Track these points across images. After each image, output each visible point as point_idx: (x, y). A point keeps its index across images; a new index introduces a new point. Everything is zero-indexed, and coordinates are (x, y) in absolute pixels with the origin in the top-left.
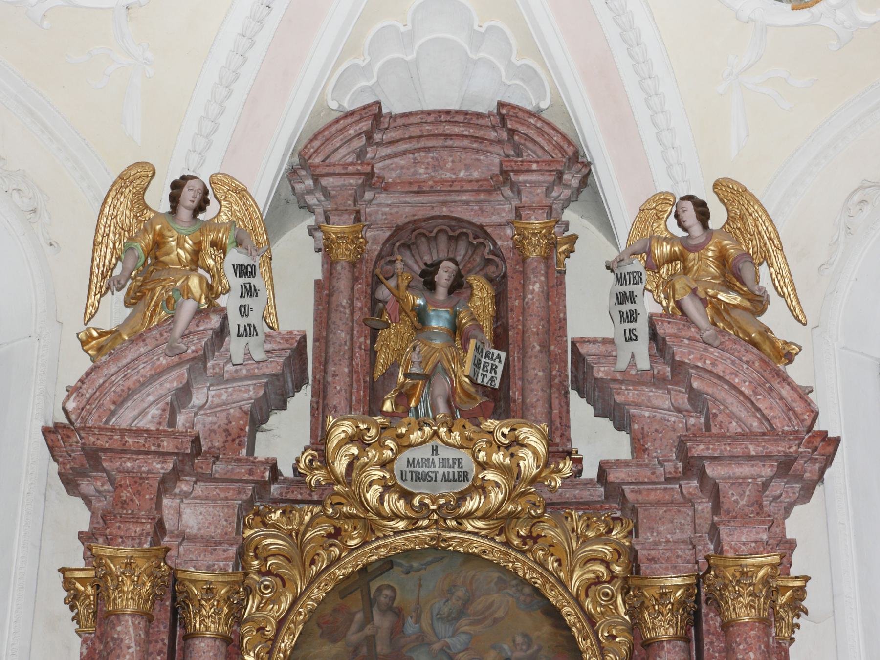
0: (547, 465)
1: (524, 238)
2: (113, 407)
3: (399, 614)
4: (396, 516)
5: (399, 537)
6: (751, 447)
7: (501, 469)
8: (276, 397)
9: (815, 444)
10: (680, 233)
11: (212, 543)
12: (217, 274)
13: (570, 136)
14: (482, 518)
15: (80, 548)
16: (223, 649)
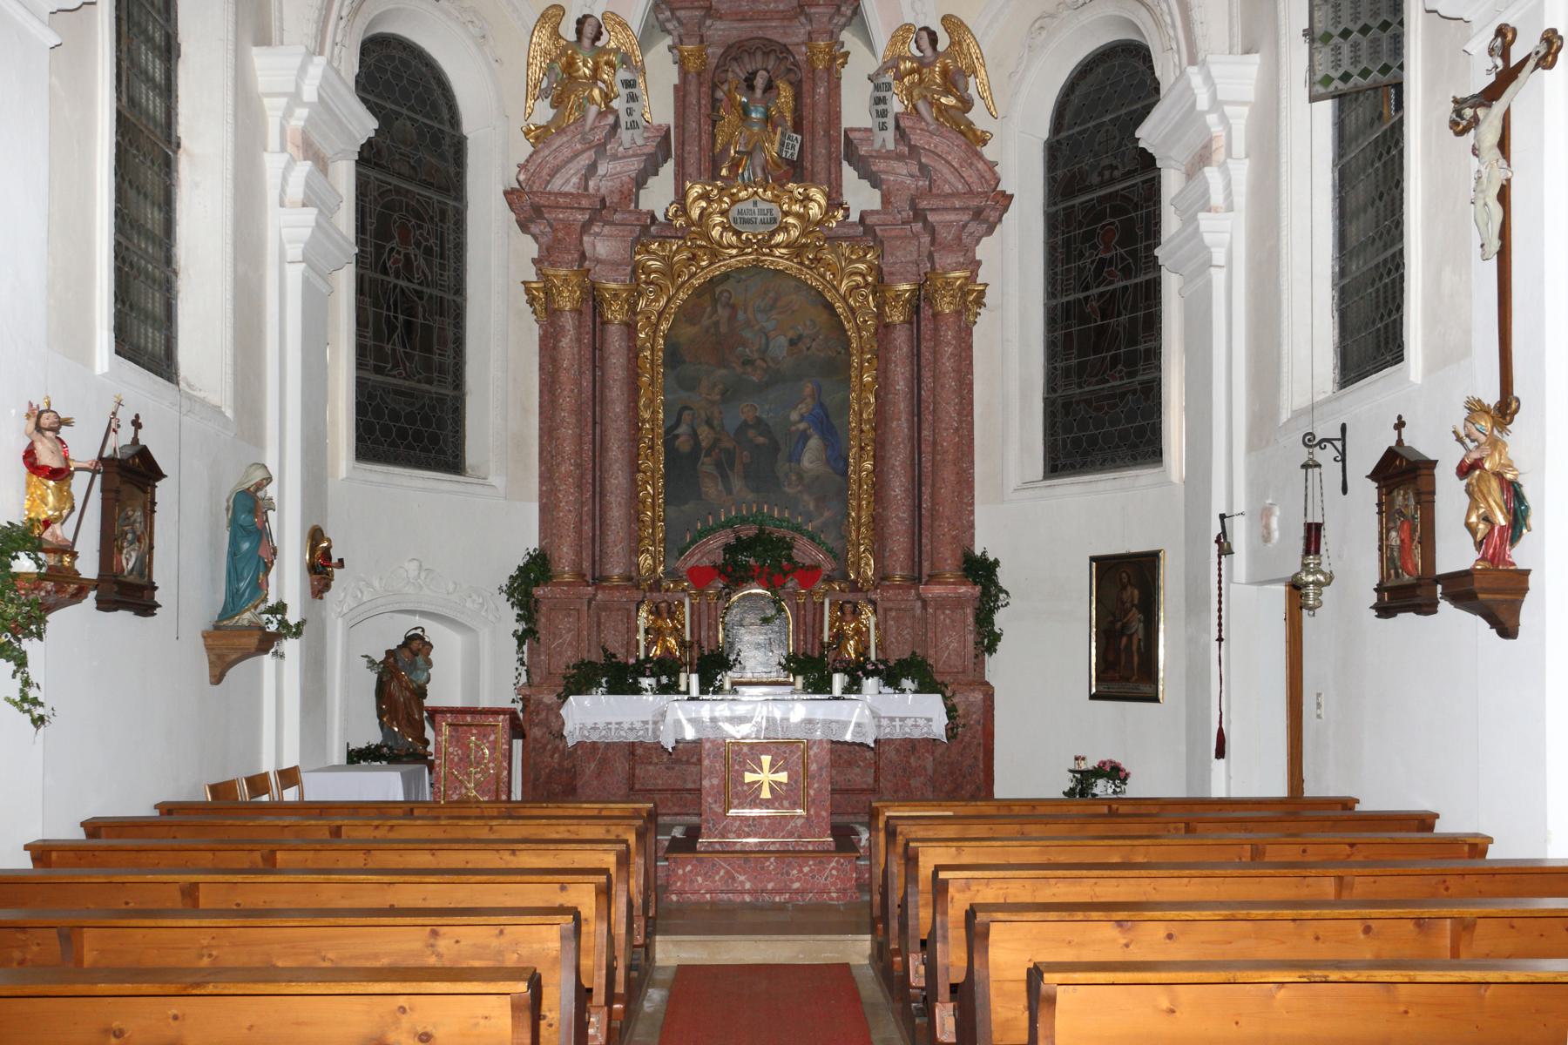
3: (734, 308)
4: (731, 246)
5: (732, 259)
7: (798, 215)
8: (651, 167)
10: (918, 54)
11: (615, 265)
12: (610, 85)
15: (534, 269)
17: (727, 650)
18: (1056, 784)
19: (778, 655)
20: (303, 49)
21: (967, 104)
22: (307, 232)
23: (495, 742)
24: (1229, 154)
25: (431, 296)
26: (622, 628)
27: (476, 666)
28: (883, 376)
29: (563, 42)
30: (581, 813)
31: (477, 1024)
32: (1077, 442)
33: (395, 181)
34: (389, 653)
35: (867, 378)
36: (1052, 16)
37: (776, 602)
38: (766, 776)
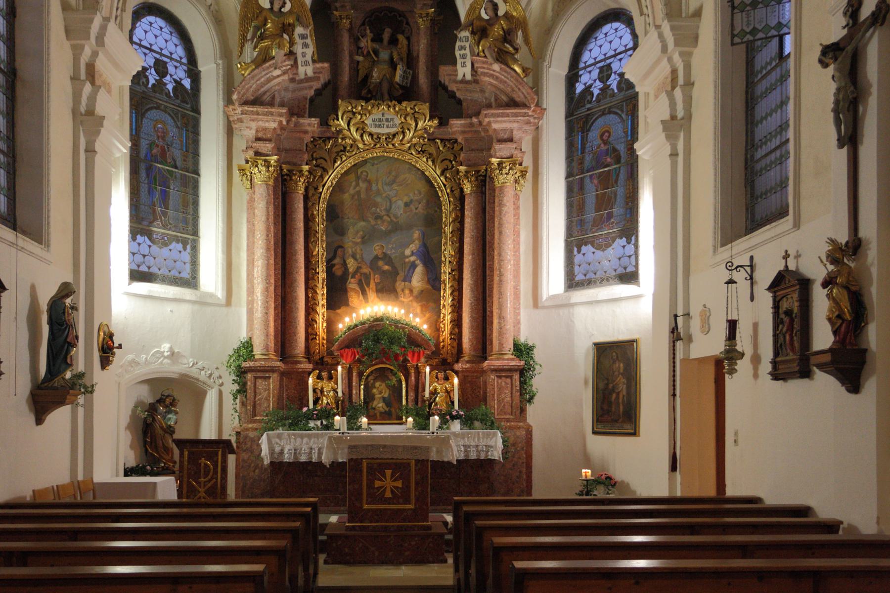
3: (369, 182)
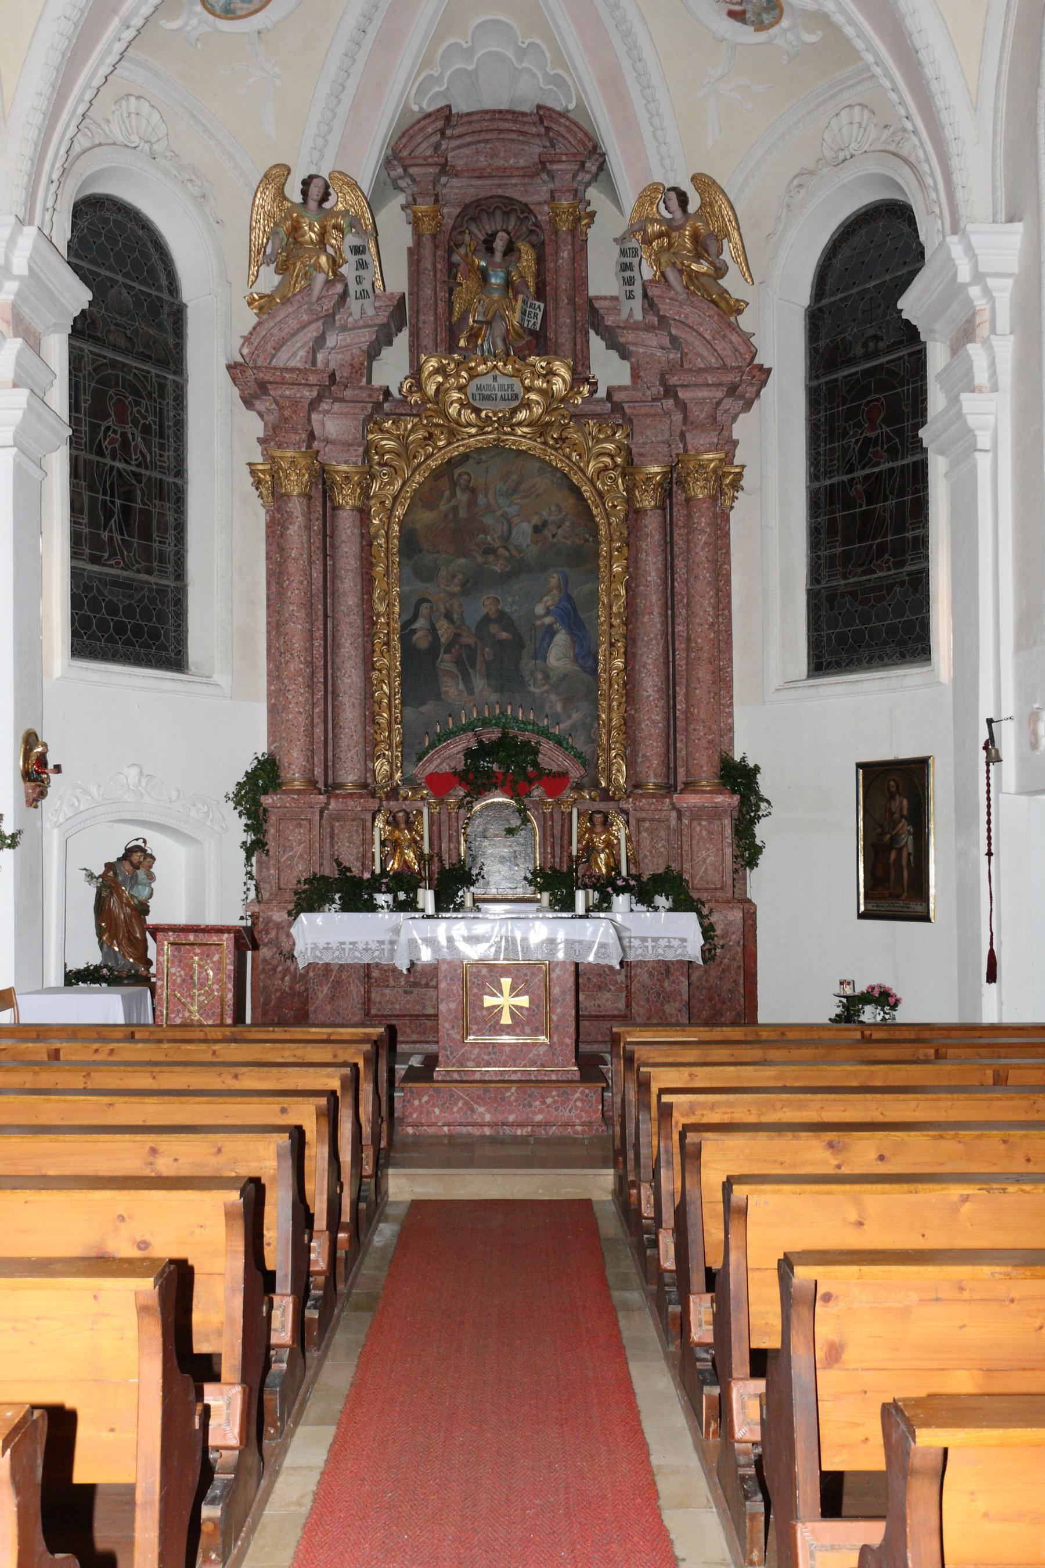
0: (572, 388)
1: (557, 215)
2: (273, 352)
3: (473, 491)
4: (469, 425)
5: (472, 439)
6: (709, 378)
9: (754, 373)
11: (347, 445)
12: (338, 250)
13: (591, 133)
14: (526, 426)
15: (259, 449)
16: (358, 517)
17: (469, 860)
18: (824, 1009)
19: (522, 870)
20: (13, 220)
21: (720, 271)
22: (18, 415)
23: (220, 962)
24: (993, 331)
25: (150, 478)
26: (357, 839)
27: (201, 881)
28: (633, 566)
29: (287, 204)
30: (309, 1037)
31: (193, 1233)
32: (842, 638)
33: (110, 354)
34: (109, 866)
35: (617, 569)
36: (812, 173)
37: (522, 812)
38: (505, 1000)
